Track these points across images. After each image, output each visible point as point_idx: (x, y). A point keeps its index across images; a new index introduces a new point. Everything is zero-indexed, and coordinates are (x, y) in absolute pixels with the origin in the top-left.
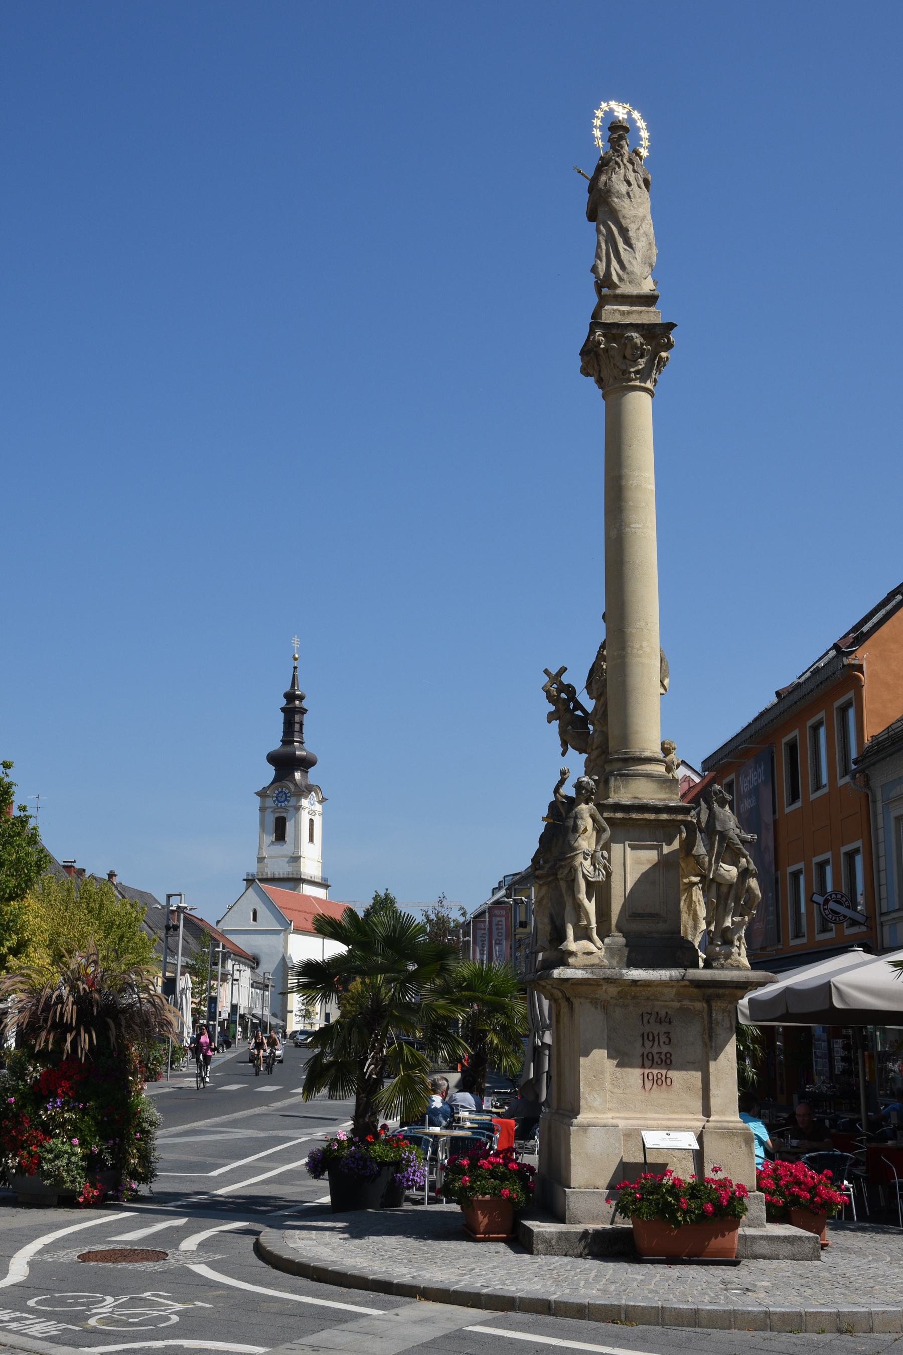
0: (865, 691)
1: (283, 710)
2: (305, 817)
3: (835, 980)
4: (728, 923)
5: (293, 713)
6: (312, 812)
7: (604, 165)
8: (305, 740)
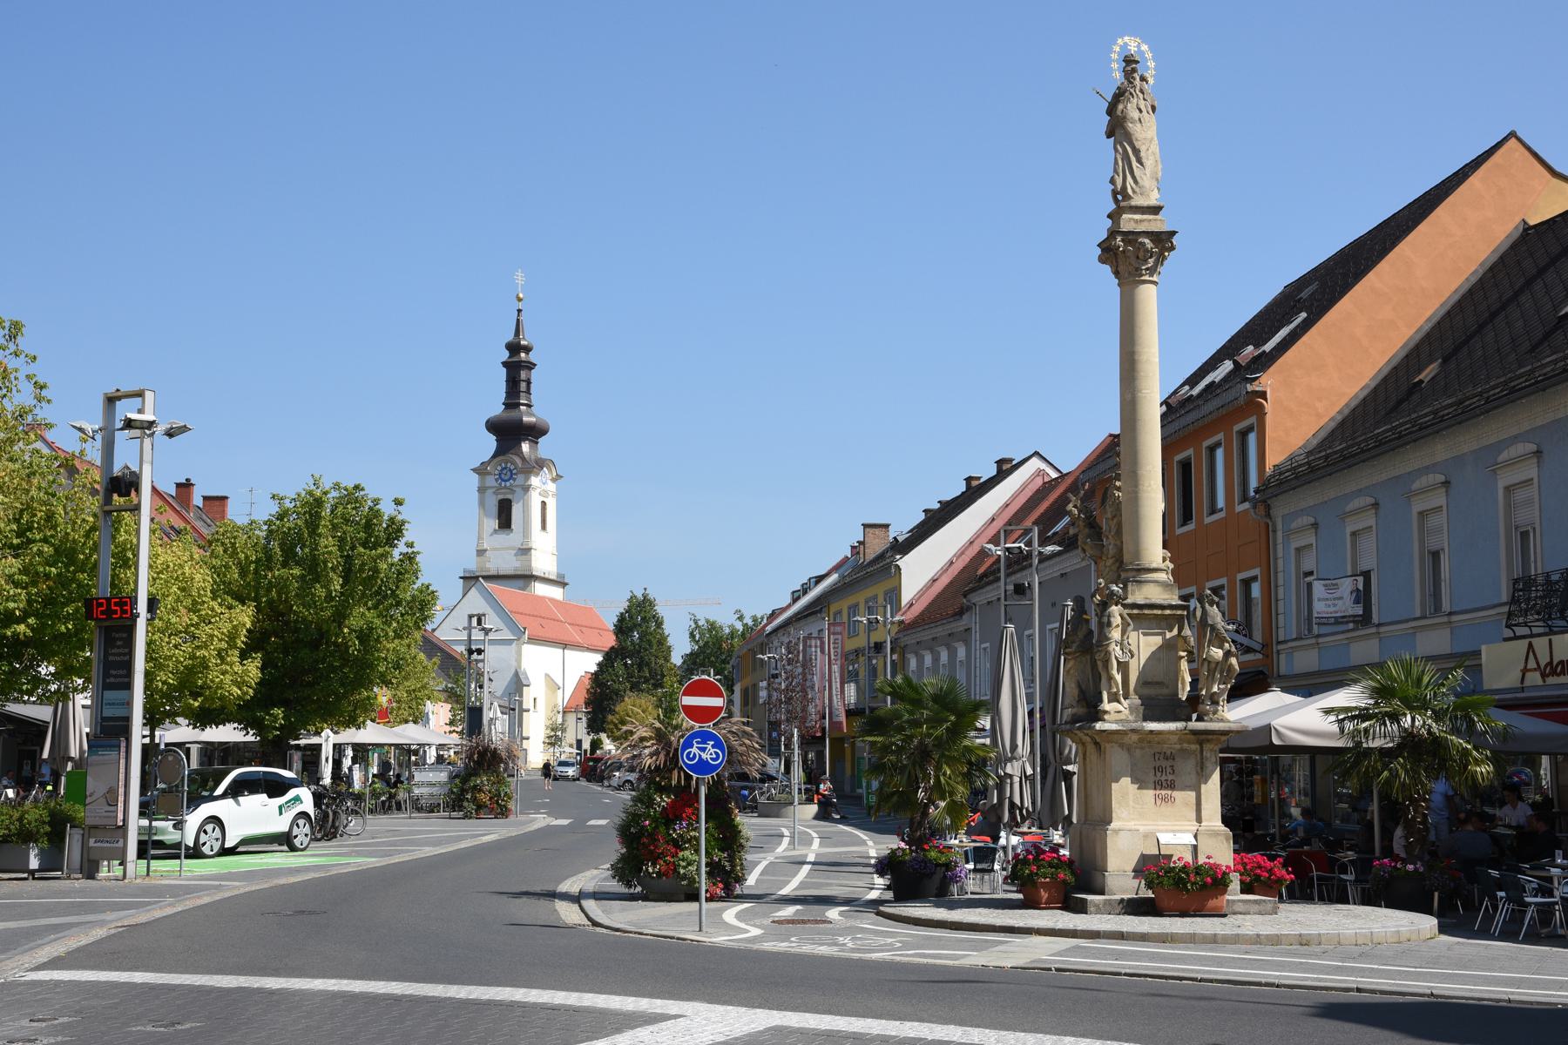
0: (1269, 419)
1: (505, 364)
2: (535, 499)
3: (1274, 723)
4: (1215, 689)
5: (517, 368)
6: (544, 493)
7: (1120, 95)
8: (533, 402)
